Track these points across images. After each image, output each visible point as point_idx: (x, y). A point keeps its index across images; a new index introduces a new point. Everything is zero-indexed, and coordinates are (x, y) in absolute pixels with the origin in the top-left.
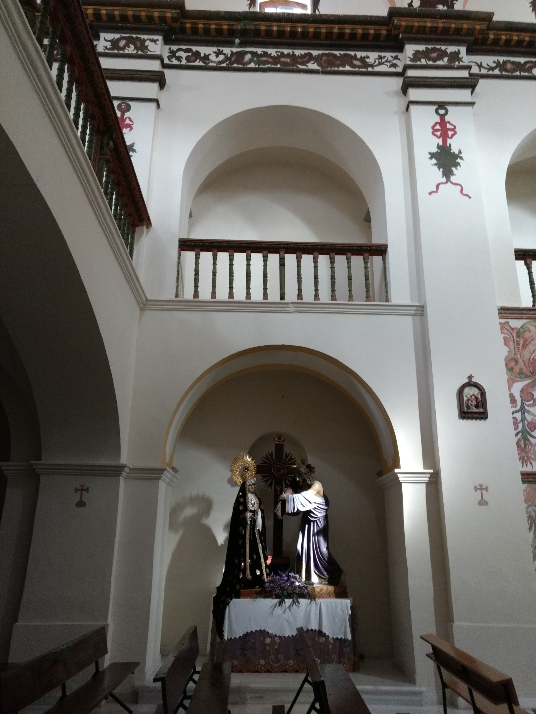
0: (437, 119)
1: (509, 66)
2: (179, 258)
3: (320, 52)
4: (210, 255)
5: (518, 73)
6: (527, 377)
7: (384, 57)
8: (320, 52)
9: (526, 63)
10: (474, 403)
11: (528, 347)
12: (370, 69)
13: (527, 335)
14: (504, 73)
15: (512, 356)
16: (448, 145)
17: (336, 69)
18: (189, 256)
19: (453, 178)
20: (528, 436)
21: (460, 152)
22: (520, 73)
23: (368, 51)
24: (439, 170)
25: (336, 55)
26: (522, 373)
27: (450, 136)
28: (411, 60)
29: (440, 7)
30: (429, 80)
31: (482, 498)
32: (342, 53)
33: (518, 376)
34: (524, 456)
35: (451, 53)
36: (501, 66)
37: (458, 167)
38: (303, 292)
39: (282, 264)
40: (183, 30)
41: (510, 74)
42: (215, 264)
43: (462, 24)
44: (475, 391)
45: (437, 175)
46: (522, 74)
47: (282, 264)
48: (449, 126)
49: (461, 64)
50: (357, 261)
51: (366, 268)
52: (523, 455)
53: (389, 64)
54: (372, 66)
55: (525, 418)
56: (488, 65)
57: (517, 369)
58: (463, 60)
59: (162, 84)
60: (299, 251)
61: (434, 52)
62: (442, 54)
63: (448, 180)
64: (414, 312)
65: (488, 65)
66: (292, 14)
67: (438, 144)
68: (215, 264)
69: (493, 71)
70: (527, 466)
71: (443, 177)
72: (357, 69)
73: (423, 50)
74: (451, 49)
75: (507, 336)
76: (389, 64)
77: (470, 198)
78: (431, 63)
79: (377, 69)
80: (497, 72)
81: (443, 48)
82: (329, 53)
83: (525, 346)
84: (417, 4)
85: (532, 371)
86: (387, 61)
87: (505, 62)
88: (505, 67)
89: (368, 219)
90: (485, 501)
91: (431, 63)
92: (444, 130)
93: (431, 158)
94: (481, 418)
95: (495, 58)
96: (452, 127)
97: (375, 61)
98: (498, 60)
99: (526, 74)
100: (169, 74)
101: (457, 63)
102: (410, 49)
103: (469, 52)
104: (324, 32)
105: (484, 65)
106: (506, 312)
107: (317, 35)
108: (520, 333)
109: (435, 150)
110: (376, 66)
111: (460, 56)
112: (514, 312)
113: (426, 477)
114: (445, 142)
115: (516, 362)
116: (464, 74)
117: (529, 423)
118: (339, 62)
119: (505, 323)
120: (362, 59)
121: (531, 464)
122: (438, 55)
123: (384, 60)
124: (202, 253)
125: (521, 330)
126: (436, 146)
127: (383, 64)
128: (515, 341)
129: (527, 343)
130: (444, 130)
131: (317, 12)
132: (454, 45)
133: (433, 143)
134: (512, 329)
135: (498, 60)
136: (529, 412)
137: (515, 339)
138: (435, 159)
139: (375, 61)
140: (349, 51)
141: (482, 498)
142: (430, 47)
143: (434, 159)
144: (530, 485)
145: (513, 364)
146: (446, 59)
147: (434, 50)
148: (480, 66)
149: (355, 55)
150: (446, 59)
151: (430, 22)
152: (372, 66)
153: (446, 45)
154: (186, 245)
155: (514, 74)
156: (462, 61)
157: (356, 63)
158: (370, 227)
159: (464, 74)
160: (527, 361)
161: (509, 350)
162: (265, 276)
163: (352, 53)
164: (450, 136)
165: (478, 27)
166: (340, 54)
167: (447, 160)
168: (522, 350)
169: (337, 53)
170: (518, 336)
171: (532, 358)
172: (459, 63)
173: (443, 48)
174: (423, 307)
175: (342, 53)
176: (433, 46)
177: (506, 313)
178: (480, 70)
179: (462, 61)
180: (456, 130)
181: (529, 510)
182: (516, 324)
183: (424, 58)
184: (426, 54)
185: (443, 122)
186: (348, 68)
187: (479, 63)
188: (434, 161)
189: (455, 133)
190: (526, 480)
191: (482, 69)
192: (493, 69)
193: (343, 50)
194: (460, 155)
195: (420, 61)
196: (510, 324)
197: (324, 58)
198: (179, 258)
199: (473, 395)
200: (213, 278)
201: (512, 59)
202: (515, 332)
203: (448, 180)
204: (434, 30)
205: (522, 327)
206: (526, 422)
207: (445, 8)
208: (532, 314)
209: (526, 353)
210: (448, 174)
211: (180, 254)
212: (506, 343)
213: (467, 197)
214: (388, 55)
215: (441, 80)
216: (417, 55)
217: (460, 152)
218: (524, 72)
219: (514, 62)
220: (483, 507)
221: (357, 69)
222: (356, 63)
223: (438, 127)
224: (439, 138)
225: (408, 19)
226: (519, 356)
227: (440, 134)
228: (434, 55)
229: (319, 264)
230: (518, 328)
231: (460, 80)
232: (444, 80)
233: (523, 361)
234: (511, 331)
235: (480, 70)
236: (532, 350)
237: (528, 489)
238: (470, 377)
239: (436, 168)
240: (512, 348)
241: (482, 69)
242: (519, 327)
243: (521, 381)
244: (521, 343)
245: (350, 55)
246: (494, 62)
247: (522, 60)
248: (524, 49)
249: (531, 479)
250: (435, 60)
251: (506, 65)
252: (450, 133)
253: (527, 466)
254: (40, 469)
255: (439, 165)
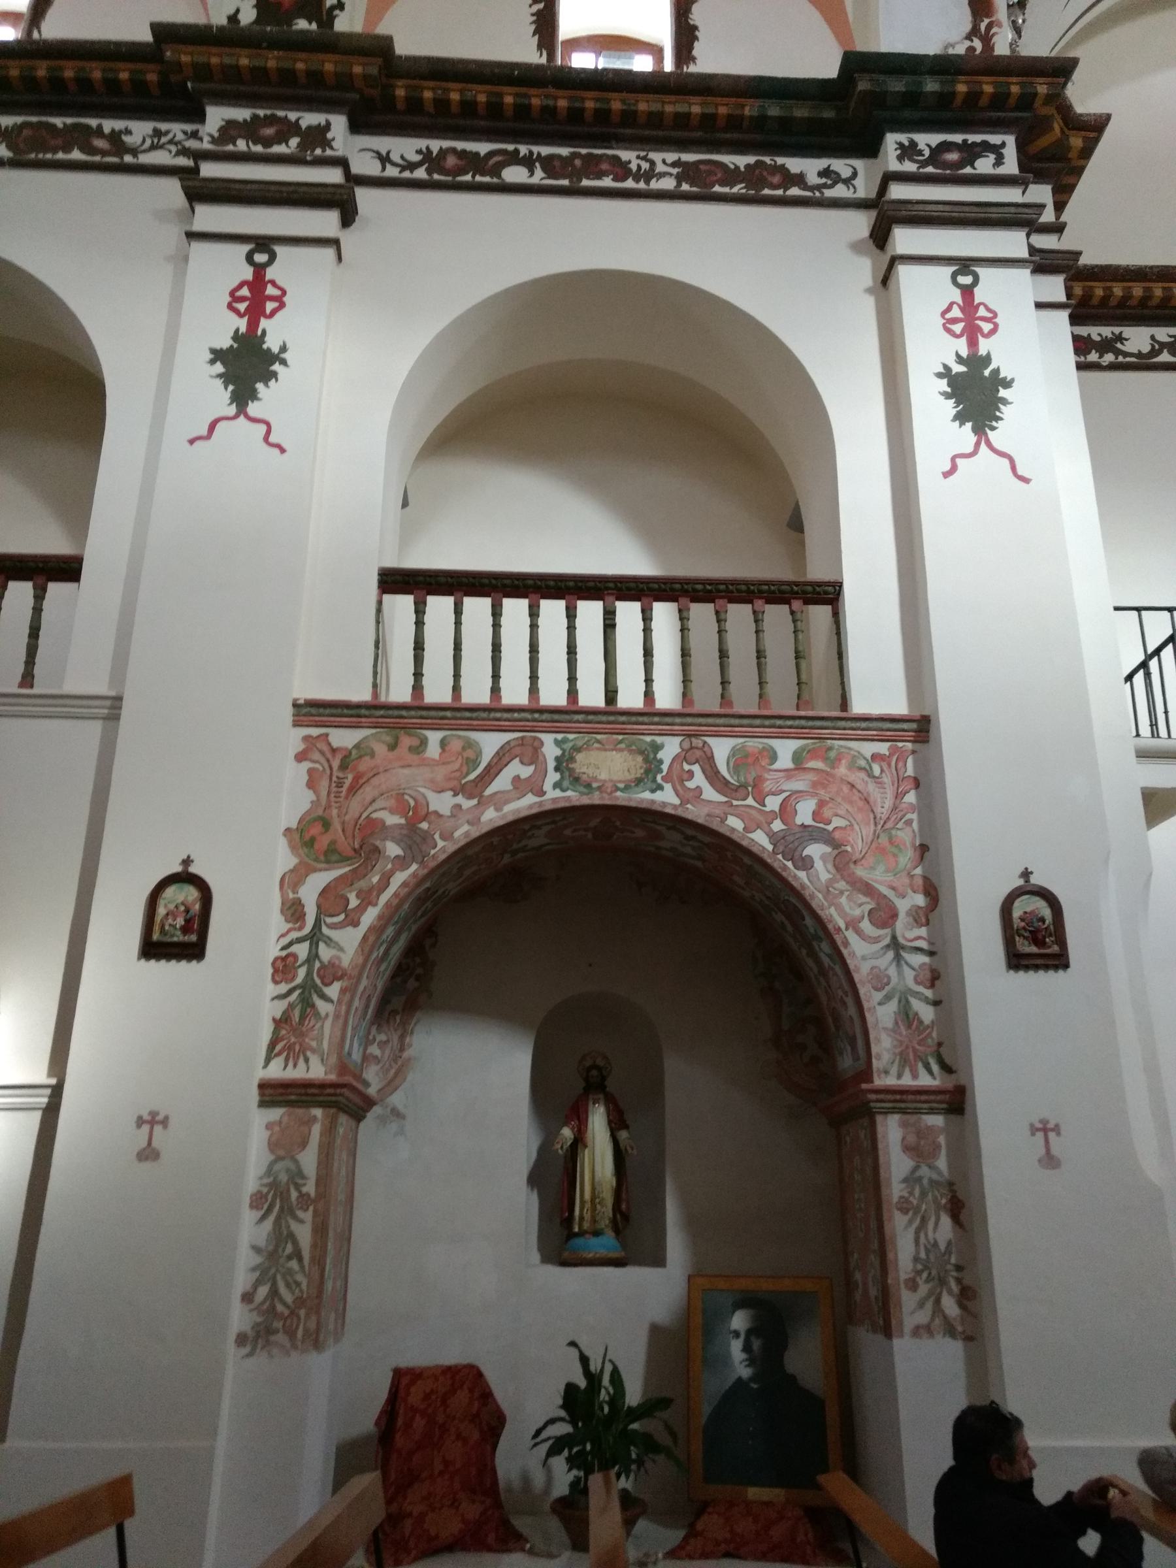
0: (248, 273)
1: (451, 161)
2: (379, 610)
3: (19, 119)
4: (522, 604)
5: (468, 178)
6: (344, 859)
7: (167, 132)
8: (19, 119)
9: (491, 154)
10: (180, 921)
11: (361, 791)
12: (128, 159)
13: (365, 765)
14: (436, 176)
15: (320, 812)
16: (259, 333)
17: (49, 156)
18: (402, 604)
19: (253, 409)
20: (315, 998)
21: (284, 349)
22: (473, 177)
23: (130, 118)
24: (226, 388)
25: (54, 126)
26: (334, 851)
27: (268, 311)
28: (214, 141)
29: (302, 24)
30: (237, 186)
31: (150, 1143)
32: (69, 121)
33: (322, 858)
34: (295, 1043)
35: (309, 128)
36: (430, 160)
37: (272, 383)
38: (37, 670)
39: (609, 625)
40: (389, 103)
41: (450, 178)
42: (496, 626)
43: (323, 62)
44: (190, 894)
45: (220, 398)
46: (478, 178)
47: (609, 625)
48: (270, 291)
49: (329, 152)
50: (776, 615)
51: (720, 632)
52: (293, 1040)
53: (174, 149)
54: (134, 152)
55: (317, 956)
56: (402, 157)
57: (324, 842)
58: (334, 144)
59: (348, 218)
60: (459, 590)
61: (271, 124)
62: (288, 130)
63: (242, 410)
64: (106, 711)
65: (402, 157)
66: (630, 72)
67: (237, 330)
68: (496, 626)
69: (412, 172)
70: (295, 1066)
71: (231, 403)
72: (97, 158)
73: (245, 121)
74: (310, 119)
75: (317, 766)
76: (174, 149)
77: (283, 451)
78: (258, 149)
79: (145, 159)
80: (421, 173)
81: (292, 116)
82: (40, 123)
83: (354, 789)
84: (248, 16)
85: (357, 846)
86: (171, 142)
87: (443, 152)
88: (442, 163)
89: (796, 524)
90: (154, 1150)
91: (258, 149)
92: (257, 298)
93: (212, 362)
94: (1056, 968)
95: (422, 143)
96: (277, 292)
97: (144, 141)
98: (428, 148)
99: (487, 179)
100: (364, 197)
101: (318, 151)
102: (216, 116)
103: (356, 127)
104: (643, 112)
105: (395, 157)
106: (311, 712)
107: (734, 122)
108: (347, 760)
109: (225, 342)
110: (144, 151)
111: (329, 136)
112: (339, 711)
113: (42, 1096)
114: (253, 324)
115: (326, 824)
116: (334, 176)
117: (323, 967)
118: (59, 142)
119: (318, 737)
120: (115, 137)
121: (307, 1060)
122: (277, 133)
123: (164, 140)
124: (431, 599)
125: (354, 752)
126: (232, 334)
127: (162, 147)
128: (334, 779)
129: (361, 781)
130: (257, 298)
131: (692, 69)
132: (319, 110)
133: (225, 328)
134: (334, 751)
135: (428, 148)
136: (329, 941)
137: (335, 773)
138: (223, 363)
139: (144, 141)
140: (718, 152)
141: (150, 1143)
142: (261, 113)
143: (218, 363)
144: (291, 1110)
145: (316, 830)
146: (294, 142)
147: (271, 120)
148: (385, 159)
149: (100, 127)
150: (294, 142)
151: (247, 57)
152: (134, 152)
153: (298, 110)
154: (394, 581)
155: (459, 179)
156: (332, 148)
157: (100, 143)
158: (802, 543)
159: (334, 176)
160: (353, 822)
161: (314, 798)
162: (496, 648)
163: (93, 122)
164: (268, 311)
165: (357, 69)
166: (65, 124)
167: (247, 366)
168: (346, 798)
169: (58, 122)
170: (343, 767)
171: (364, 816)
172: (324, 151)
173: (292, 116)
174: (119, 699)
175: (69, 121)
176: (269, 112)
177: (320, 715)
178: (384, 169)
179: (332, 148)
180: (229, 299)
181: (277, 1167)
182: (344, 738)
183: (243, 137)
184: (249, 130)
185: (258, 282)
186: (76, 155)
187: (384, 153)
188: (219, 368)
189: (282, 305)
190: (281, 1098)
191: (388, 166)
192: (412, 166)
193: (71, 116)
194: (283, 356)
195: (235, 144)
196: (330, 739)
197: (26, 132)
198: (379, 610)
199: (183, 904)
200: (29, 645)
201: (460, 145)
202: (339, 757)
203: (242, 410)
204: (260, 74)
205: (357, 746)
206: (317, 965)
207: (314, 26)
208: (382, 717)
209: (355, 806)
210: (243, 396)
211: (380, 603)
212: (311, 784)
213: (276, 451)
214: (177, 129)
215: (262, 186)
216: (229, 131)
217: (284, 349)
218: (482, 175)
219: (464, 151)
220: (147, 1165)
221: (97, 158)
222: (100, 143)
223: (245, 292)
224: (241, 315)
225: (227, 50)
226: (335, 812)
227: (247, 309)
228: (269, 131)
229: (654, 625)
230: (346, 749)
231: (242, 186)
232: (273, 188)
233: (343, 823)
234: (329, 756)
235: (384, 169)
236: (369, 798)
237: (285, 1119)
238: (187, 862)
239: (219, 383)
240: (324, 793)
241: (388, 166)
242: (350, 747)
243: (326, 870)
244: (348, 782)
245: (88, 127)
246: (419, 152)
247: (483, 148)
248: (482, 123)
249: (293, 1097)
250: (268, 143)
251: (445, 158)
252: (270, 306)
253: (295, 1066)
254: (878, 1101)
255: (227, 378)
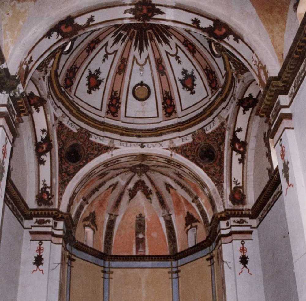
48: (245, 249)
